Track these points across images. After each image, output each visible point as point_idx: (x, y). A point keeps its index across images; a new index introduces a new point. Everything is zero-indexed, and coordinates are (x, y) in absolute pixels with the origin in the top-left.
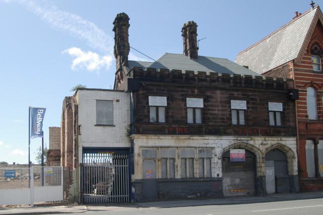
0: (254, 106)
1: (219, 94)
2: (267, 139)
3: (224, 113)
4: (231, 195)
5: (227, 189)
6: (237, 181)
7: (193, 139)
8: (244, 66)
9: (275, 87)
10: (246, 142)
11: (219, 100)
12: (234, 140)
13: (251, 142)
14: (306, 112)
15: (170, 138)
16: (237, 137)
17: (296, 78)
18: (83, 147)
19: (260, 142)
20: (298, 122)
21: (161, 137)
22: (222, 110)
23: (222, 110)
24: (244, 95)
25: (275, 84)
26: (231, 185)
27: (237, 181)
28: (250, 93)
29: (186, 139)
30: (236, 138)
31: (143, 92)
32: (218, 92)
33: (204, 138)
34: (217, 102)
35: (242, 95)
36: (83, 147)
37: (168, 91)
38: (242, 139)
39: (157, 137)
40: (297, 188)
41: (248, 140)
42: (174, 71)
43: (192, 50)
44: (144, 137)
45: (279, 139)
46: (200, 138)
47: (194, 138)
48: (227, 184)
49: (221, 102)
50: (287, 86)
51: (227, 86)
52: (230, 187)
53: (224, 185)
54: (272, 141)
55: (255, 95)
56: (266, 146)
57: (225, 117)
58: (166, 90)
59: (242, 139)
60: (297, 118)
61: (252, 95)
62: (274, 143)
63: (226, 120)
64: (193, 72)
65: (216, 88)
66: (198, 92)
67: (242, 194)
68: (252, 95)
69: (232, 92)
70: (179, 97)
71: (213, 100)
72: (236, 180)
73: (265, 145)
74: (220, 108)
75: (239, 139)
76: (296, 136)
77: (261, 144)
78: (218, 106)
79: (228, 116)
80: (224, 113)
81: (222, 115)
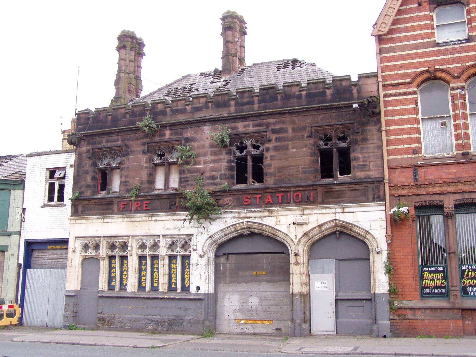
0: (279, 144)
1: (209, 132)
2: (306, 212)
3: (216, 165)
4: (239, 331)
5: (232, 317)
6: (254, 302)
7: (156, 221)
8: (202, 74)
9: (109, 124)
10: (259, 221)
11: (207, 143)
12: (234, 218)
13: (269, 221)
14: (418, 141)
15: (120, 220)
16: (303, 210)
17: (383, 69)
18: (25, 240)
19: (291, 219)
20: (389, 168)
21: (106, 220)
22: (214, 161)
23: (214, 161)
24: (259, 125)
25: (329, 92)
26: (239, 311)
27: (254, 302)
28: (272, 120)
29: (144, 221)
30: (237, 215)
31: (89, 148)
32: (207, 129)
33: (175, 217)
34: (203, 146)
35: (254, 126)
36: (25, 240)
37: (122, 140)
38: (249, 215)
39: (100, 221)
40: (384, 324)
41: (261, 217)
42: (336, 80)
43: (232, 55)
44: (84, 221)
45: (339, 210)
46: (168, 218)
47: (159, 218)
48: (233, 308)
49: (212, 146)
50: (359, 92)
51: (224, 113)
52: (239, 315)
53: (226, 308)
54: (321, 217)
55: (283, 122)
56: (306, 229)
57: (217, 174)
58: (120, 140)
59: (249, 215)
60: (386, 158)
61: (274, 124)
62: (323, 219)
63: (218, 180)
64: (348, 79)
65: (202, 122)
66: (171, 134)
67: (263, 330)
68: (274, 124)
69: (233, 125)
70: (138, 149)
71: (195, 144)
72: (251, 299)
73: (301, 224)
74: (209, 158)
75: (243, 215)
76: (384, 200)
77: (294, 223)
78: (205, 154)
79: (223, 172)
80: (216, 165)
81: (213, 170)
